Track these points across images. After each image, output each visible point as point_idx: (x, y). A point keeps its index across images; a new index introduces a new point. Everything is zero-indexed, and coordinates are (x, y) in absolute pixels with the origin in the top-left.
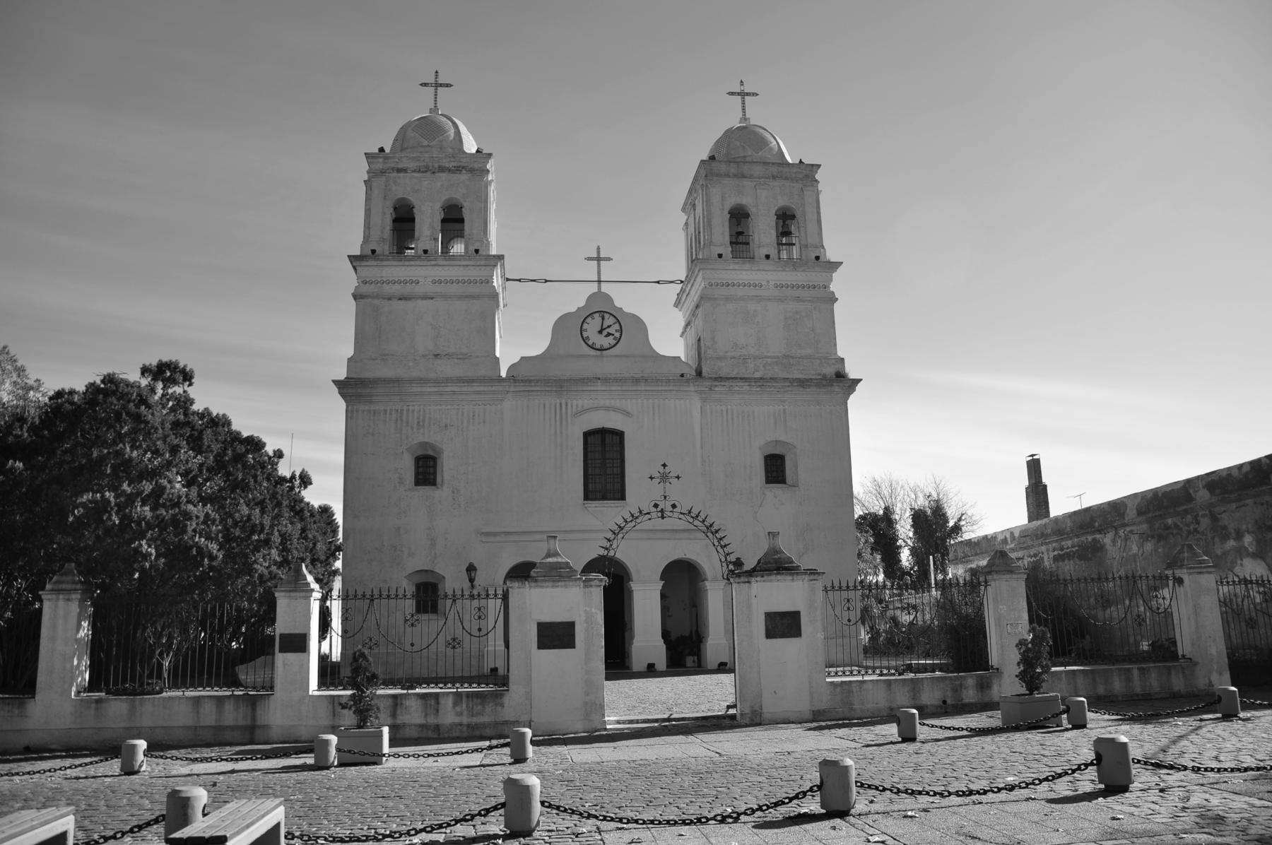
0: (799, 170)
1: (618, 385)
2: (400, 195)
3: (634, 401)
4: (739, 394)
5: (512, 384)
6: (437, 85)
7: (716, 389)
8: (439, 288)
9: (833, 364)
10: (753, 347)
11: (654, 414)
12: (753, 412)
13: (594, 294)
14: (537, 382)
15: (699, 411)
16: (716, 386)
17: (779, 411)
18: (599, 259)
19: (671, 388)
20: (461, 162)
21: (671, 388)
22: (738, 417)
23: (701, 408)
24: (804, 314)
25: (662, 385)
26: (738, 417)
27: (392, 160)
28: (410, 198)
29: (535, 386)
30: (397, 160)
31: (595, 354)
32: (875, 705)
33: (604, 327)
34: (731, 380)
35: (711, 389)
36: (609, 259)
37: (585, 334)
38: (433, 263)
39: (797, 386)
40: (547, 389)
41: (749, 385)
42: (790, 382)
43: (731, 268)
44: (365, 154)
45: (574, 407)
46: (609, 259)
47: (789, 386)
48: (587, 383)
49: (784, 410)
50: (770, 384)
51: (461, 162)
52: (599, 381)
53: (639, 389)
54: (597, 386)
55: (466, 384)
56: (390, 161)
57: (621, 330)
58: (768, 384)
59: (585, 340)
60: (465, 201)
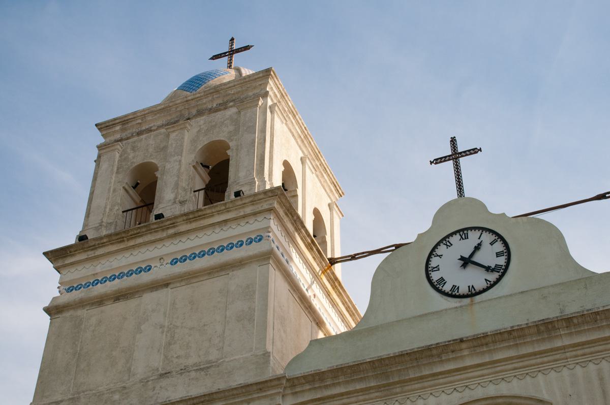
1: (509, 347)
2: (139, 160)
3: (553, 374)
5: (289, 391)
6: (232, 52)
8: (180, 268)
13: (448, 205)
14: (336, 377)
18: (455, 156)
20: (227, 95)
27: (134, 123)
28: (153, 161)
29: (334, 385)
30: (140, 121)
31: (458, 305)
32: (129, 171)
33: (235, 47)
36: (453, 141)
37: (435, 276)
38: (171, 231)
40: (358, 386)
44: (96, 125)
46: (453, 141)
48: (439, 356)
51: (227, 95)
52: (464, 346)
53: (559, 343)
54: (462, 357)
57: (507, 252)
59: (436, 286)
60: (232, 140)
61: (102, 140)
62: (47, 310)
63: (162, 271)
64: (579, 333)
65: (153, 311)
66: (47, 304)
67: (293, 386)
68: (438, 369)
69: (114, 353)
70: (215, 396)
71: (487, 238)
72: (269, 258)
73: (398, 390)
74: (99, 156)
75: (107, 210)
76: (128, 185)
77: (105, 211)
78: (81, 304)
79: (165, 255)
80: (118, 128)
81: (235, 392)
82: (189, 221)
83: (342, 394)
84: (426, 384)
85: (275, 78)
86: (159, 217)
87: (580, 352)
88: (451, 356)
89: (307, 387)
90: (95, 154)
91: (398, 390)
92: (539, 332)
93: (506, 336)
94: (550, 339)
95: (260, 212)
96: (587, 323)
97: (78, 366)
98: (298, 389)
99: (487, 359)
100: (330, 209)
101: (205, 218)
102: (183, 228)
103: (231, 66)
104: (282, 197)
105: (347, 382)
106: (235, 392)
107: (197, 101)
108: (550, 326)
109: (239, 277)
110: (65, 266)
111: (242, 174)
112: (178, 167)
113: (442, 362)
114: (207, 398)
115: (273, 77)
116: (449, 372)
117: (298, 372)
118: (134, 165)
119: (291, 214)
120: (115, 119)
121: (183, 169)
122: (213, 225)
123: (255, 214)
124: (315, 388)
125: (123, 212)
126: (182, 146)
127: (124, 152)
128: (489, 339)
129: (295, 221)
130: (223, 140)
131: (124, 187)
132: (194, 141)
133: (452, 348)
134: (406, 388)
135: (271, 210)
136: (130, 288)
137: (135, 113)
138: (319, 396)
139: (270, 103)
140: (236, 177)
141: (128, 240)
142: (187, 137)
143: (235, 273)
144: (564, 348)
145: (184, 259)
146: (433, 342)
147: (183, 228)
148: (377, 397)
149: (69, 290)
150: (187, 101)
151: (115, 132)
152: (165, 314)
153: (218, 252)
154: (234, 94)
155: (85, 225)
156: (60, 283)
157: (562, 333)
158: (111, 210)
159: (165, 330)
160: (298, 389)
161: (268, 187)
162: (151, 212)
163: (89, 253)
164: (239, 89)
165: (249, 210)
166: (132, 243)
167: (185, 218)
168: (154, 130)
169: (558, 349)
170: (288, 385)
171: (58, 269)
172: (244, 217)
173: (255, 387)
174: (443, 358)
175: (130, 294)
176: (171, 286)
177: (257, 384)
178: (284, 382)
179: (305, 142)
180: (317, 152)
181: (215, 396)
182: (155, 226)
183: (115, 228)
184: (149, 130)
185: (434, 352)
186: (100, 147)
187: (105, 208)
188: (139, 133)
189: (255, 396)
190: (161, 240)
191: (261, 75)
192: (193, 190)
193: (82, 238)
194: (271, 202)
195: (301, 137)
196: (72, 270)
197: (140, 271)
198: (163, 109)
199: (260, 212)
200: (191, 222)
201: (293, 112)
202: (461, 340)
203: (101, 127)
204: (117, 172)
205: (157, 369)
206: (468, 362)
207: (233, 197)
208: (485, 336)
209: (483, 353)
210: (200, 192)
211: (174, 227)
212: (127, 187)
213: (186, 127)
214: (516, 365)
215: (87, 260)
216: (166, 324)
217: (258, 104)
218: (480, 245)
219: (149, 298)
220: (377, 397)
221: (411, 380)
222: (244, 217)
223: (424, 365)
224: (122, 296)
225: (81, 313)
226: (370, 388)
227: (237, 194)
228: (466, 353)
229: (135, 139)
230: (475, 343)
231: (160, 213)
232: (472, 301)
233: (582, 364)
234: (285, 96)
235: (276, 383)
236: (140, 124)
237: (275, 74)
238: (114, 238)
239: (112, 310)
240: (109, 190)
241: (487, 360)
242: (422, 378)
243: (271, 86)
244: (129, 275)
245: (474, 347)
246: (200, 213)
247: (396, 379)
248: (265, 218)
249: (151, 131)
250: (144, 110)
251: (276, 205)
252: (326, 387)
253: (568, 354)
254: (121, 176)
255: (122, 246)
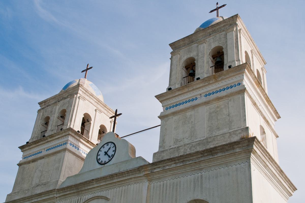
0: (225, 24)
4: (170, 171)
5: (58, 193)
7: (155, 171)
9: (240, 133)
10: (187, 139)
11: (121, 196)
12: (180, 182)
14: (67, 189)
15: (147, 188)
16: (155, 169)
17: (198, 177)
19: (131, 177)
20: (69, 93)
21: (131, 177)
22: (170, 188)
23: (148, 186)
24: (222, 107)
25: (126, 176)
26: (170, 188)
27: (47, 102)
29: (67, 191)
30: (48, 102)
34: (162, 163)
35: (152, 172)
38: (46, 141)
39: (207, 155)
41: (175, 163)
42: (202, 154)
43: (177, 94)
45: (84, 199)
47: (202, 157)
48: (89, 184)
49: (202, 176)
50: (188, 159)
51: (69, 93)
52: (94, 181)
53: (114, 181)
55: (39, 197)
56: (46, 103)
58: (187, 159)
61: (40, 108)
62: (18, 165)
63: (44, 153)
64: (119, 178)
65: (39, 166)
66: (18, 163)
67: (59, 191)
68: (89, 188)
69: (30, 178)
70: (42, 194)
71: (113, 145)
72: (66, 150)
73: (80, 193)
74: (172, 57)
75: (37, 132)
76: (43, 124)
77: (36, 133)
78: (29, 162)
79: (202, 93)
80: (43, 104)
81: (46, 193)
82: (50, 138)
83: (69, 194)
84: (86, 191)
85: (81, 86)
86: (198, 79)
87: (119, 184)
88: (92, 184)
89: (62, 192)
90: (170, 56)
91: (80, 193)
92: (110, 178)
93: (103, 178)
94: (113, 179)
95: (67, 135)
96: (121, 175)
97: (22, 182)
98: (60, 192)
99: (99, 185)
100: (262, 70)
101: (54, 137)
102: (49, 140)
103: (218, 15)
104: (72, 130)
105: (70, 191)
106: (46, 193)
107: (62, 95)
108: (112, 176)
109: (59, 155)
110: (24, 151)
111: (66, 121)
112: (53, 118)
113: (89, 185)
114: (40, 194)
115: (238, 17)
116: (91, 188)
117: (64, 186)
118: (45, 117)
119: (77, 134)
120: (43, 101)
121: (55, 119)
122: (56, 139)
123: (65, 136)
124: (63, 192)
125: (41, 132)
126: (55, 111)
127: (43, 113)
128: (99, 179)
129: (79, 136)
130: (221, 46)
131: (42, 125)
132: (59, 109)
133: (91, 182)
134: (82, 192)
135: (69, 134)
136: (35, 159)
137: (47, 99)
138: (64, 194)
139: (238, 29)
140: (227, 61)
141: (37, 143)
142: (58, 107)
143: (58, 154)
144: (115, 182)
145: (210, 94)
146: (87, 180)
147: (49, 140)
148: (76, 195)
149: (24, 158)
150: (59, 95)
151: (43, 105)
152: (42, 167)
153: (234, 87)
154: (71, 92)
155: (169, 85)
156: (22, 156)
157: (115, 178)
158: (38, 132)
159: (41, 172)
160: (60, 192)
161: (241, 63)
162: (194, 77)
163: (29, 147)
164: (72, 91)
165: (64, 134)
166: (38, 144)
167: (49, 137)
168: (51, 105)
169: (114, 183)
170: (57, 191)
171: (161, 102)
172: (63, 136)
173: (50, 192)
174: (90, 184)
175: (36, 160)
176: (44, 158)
177: (50, 191)
178: (56, 190)
179: (99, 103)
180: (105, 105)
181: (42, 194)
182: (43, 139)
183: (37, 138)
184: (50, 105)
185: (88, 183)
186: (171, 53)
187: (36, 132)
188: (48, 106)
189: (50, 194)
190: (44, 143)
191: (77, 86)
192: (57, 126)
193: (169, 89)
194: (69, 132)
195: (96, 102)
196: (25, 152)
197: (39, 153)
198: (54, 98)
199: (67, 135)
200: (51, 138)
201: (91, 95)
202: (93, 180)
203: (40, 104)
204: (41, 120)
205: (37, 184)
206: (95, 186)
207: (228, 68)
208: (98, 179)
209: (98, 183)
210: (213, 67)
211: (47, 140)
212: (43, 124)
213: (57, 105)
214: (105, 187)
215: (28, 149)
216: (41, 170)
217: (234, 30)
218: (110, 148)
219: (39, 161)
220: (76, 195)
221: (83, 190)
222: (63, 136)
223: (86, 186)
224: (34, 161)
225: (25, 166)
226: (75, 192)
227: (230, 67)
228: (95, 183)
229: (47, 108)
230: (96, 180)
231: (198, 77)
232: (104, 166)
233: (119, 187)
234: (87, 91)
235: (54, 190)
236: (49, 102)
237: (239, 17)
238: (34, 143)
239: (32, 165)
240: (38, 125)
241: (99, 185)
242: (85, 190)
243: (238, 22)
244: (195, 99)
245: (97, 181)
246: (53, 136)
247: (80, 190)
248: (239, 76)
249: (50, 105)
250: (49, 98)
251: (70, 133)
252: (66, 192)
253: (117, 184)
254: (41, 121)
255: (36, 145)
